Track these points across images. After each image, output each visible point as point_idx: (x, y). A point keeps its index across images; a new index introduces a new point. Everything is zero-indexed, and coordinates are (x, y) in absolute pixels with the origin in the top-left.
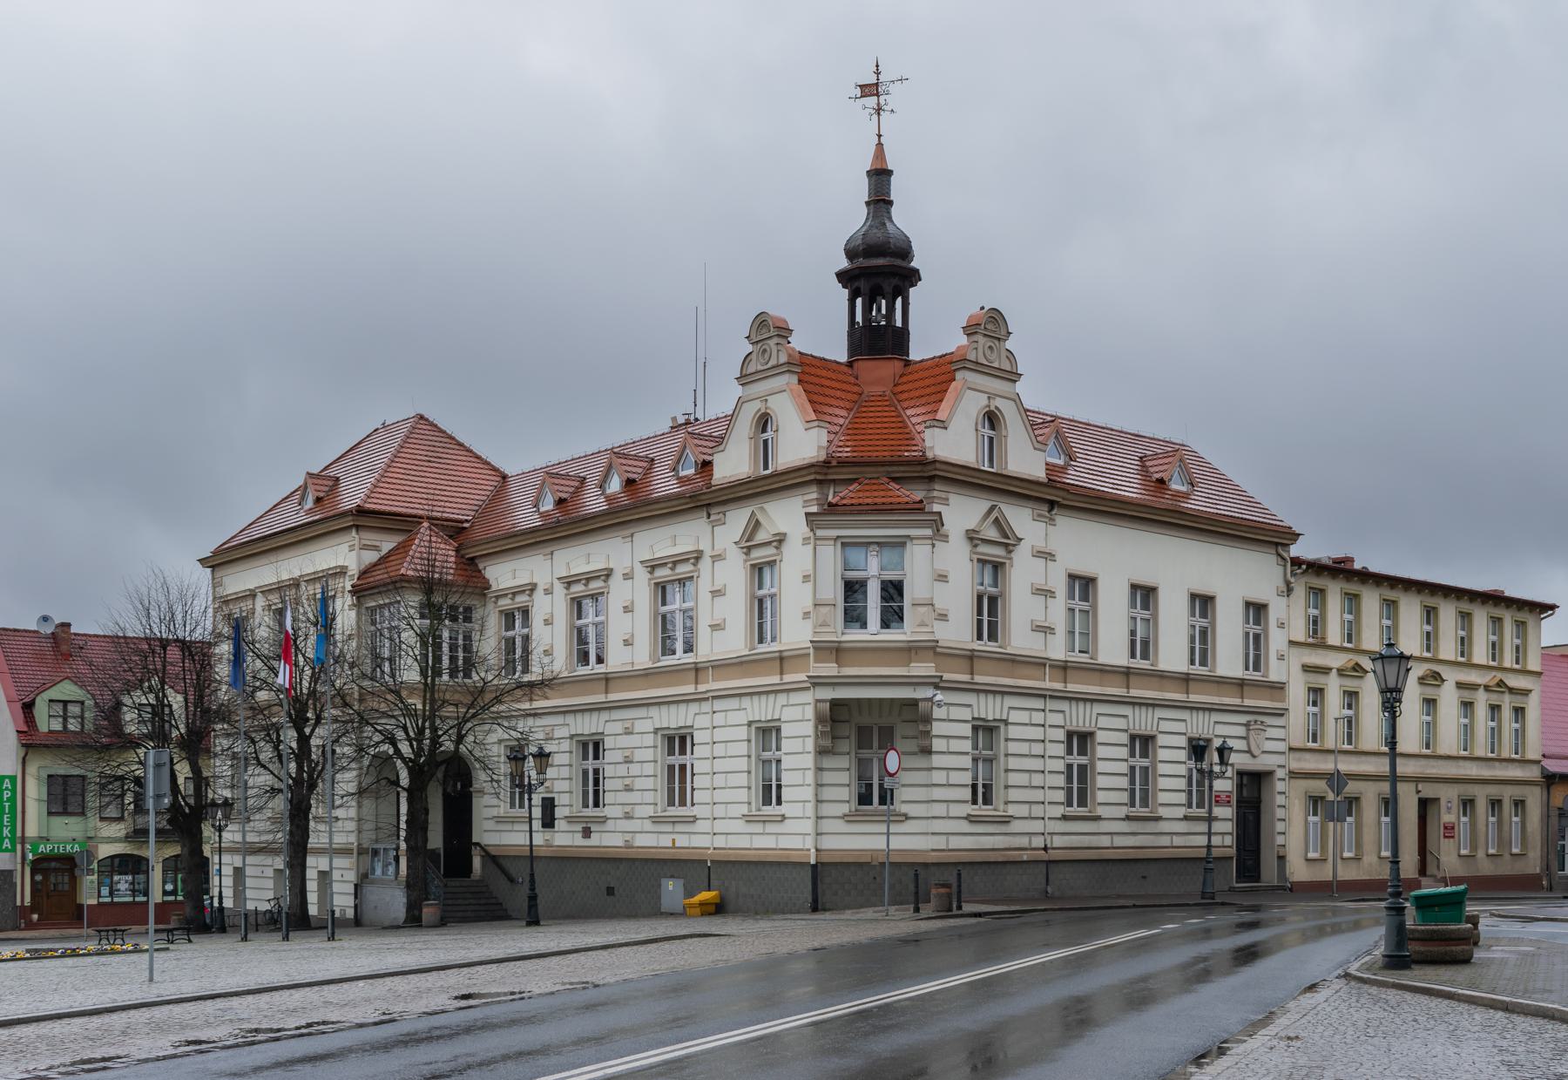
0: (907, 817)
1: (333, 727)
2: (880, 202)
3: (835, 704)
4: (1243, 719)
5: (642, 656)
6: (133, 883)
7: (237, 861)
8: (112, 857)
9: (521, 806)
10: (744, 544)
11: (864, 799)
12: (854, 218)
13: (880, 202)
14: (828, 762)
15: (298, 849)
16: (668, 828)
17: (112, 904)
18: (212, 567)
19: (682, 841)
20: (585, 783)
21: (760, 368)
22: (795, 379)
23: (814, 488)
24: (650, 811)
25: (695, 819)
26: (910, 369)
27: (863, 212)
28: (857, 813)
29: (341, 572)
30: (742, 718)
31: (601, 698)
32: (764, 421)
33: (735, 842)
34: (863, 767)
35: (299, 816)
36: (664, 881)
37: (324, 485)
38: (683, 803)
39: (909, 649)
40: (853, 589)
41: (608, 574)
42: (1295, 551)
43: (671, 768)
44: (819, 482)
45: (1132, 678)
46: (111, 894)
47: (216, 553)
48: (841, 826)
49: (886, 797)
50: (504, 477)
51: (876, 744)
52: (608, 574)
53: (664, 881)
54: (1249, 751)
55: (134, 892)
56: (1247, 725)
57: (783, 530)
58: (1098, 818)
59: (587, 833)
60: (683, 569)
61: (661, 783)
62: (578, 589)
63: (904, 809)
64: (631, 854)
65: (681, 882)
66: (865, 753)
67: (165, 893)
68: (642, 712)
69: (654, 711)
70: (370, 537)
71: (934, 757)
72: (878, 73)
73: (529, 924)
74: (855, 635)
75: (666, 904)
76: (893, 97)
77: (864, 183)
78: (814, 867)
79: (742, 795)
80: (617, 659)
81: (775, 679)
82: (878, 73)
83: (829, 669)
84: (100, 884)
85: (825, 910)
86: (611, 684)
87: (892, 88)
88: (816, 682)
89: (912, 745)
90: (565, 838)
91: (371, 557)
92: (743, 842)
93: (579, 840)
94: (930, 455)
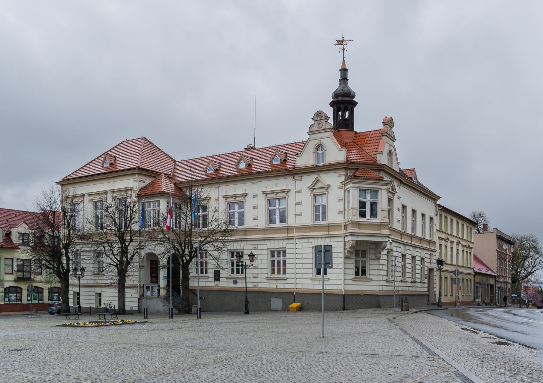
0: (372, 280)
1: (150, 241)
2: (344, 79)
3: (357, 241)
4: (429, 252)
5: (262, 223)
6: (16, 296)
7: (76, 289)
8: (9, 287)
9: (242, 273)
10: (311, 188)
11: (357, 273)
12: (335, 85)
13: (344, 79)
14: (348, 261)
15: (121, 287)
16: (275, 281)
17: (9, 304)
18: (62, 185)
19: (280, 286)
20: (233, 265)
21: (317, 129)
22: (332, 134)
23: (344, 170)
24: (266, 276)
25: (287, 279)
26: (357, 135)
27: (339, 83)
28: (355, 278)
29: (131, 189)
30: (310, 245)
31: (243, 237)
32: (318, 147)
33: (305, 287)
34: (357, 262)
35: (122, 273)
36: (272, 299)
37: (111, 158)
38: (279, 273)
39: (380, 225)
40: (363, 205)
41: (246, 195)
42: (438, 202)
43: (273, 262)
44: (345, 168)
45: (413, 239)
46: (9, 300)
47: (64, 180)
48: (351, 282)
49: (364, 272)
50: (175, 161)
51: (360, 256)
52: (246, 195)
53: (272, 299)
54: (430, 263)
55: (17, 300)
56: (430, 254)
57: (328, 183)
58: (406, 282)
59: (235, 282)
60: (238, 199)
61: (270, 266)
62: (270, 196)
63: (371, 277)
64: (257, 290)
65: (281, 299)
66: (358, 259)
67: (28, 300)
68: (262, 242)
69: (267, 242)
70: (142, 178)
71: (381, 261)
72: (343, 37)
73: (246, 313)
74: (363, 220)
75: (273, 307)
76: (348, 46)
77: (339, 73)
78: (344, 295)
79: (310, 271)
80: (291, 221)
81: (326, 233)
82: (343, 37)
83: (356, 230)
84: (5, 297)
85: (347, 310)
86: (330, 228)
87: (348, 43)
88: (352, 234)
89: (373, 257)
90: (225, 283)
91: (143, 185)
92: (311, 287)
93: (232, 285)
94: (379, 162)
